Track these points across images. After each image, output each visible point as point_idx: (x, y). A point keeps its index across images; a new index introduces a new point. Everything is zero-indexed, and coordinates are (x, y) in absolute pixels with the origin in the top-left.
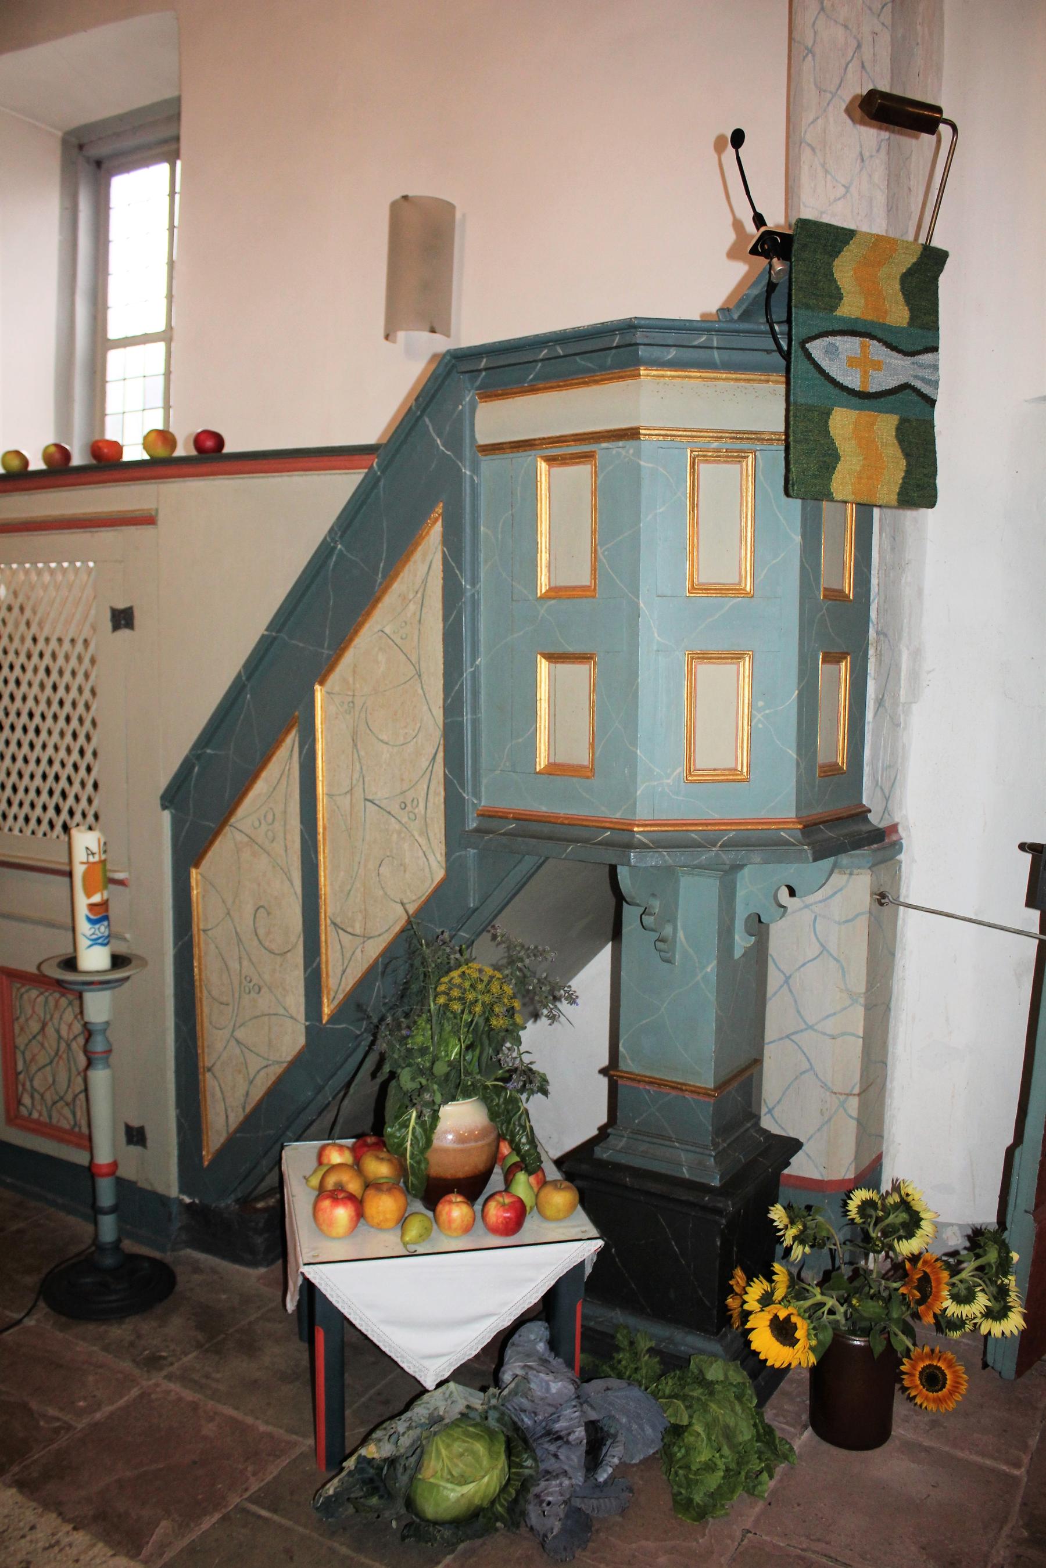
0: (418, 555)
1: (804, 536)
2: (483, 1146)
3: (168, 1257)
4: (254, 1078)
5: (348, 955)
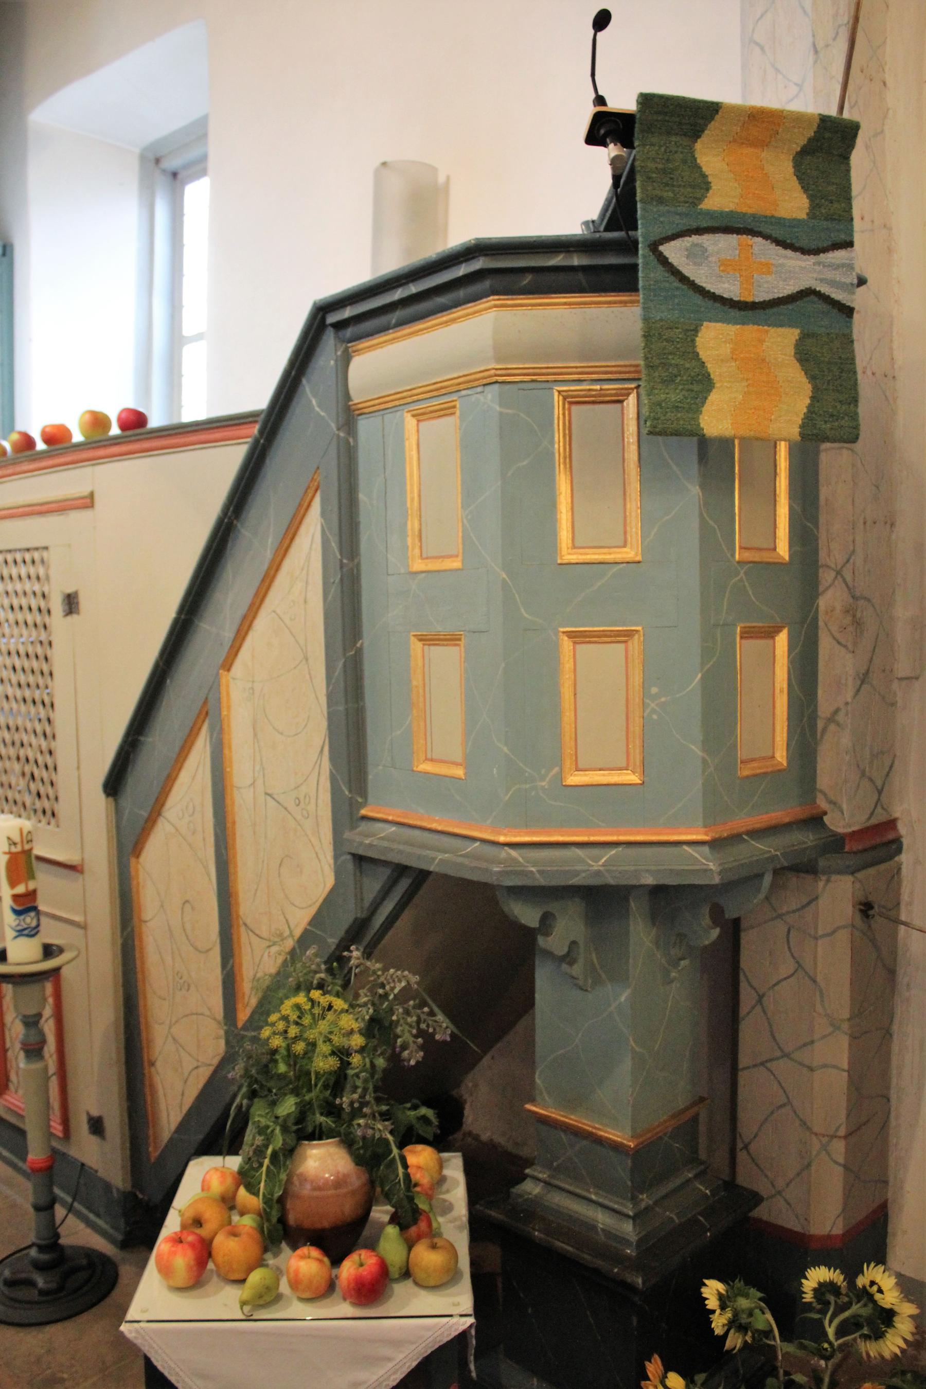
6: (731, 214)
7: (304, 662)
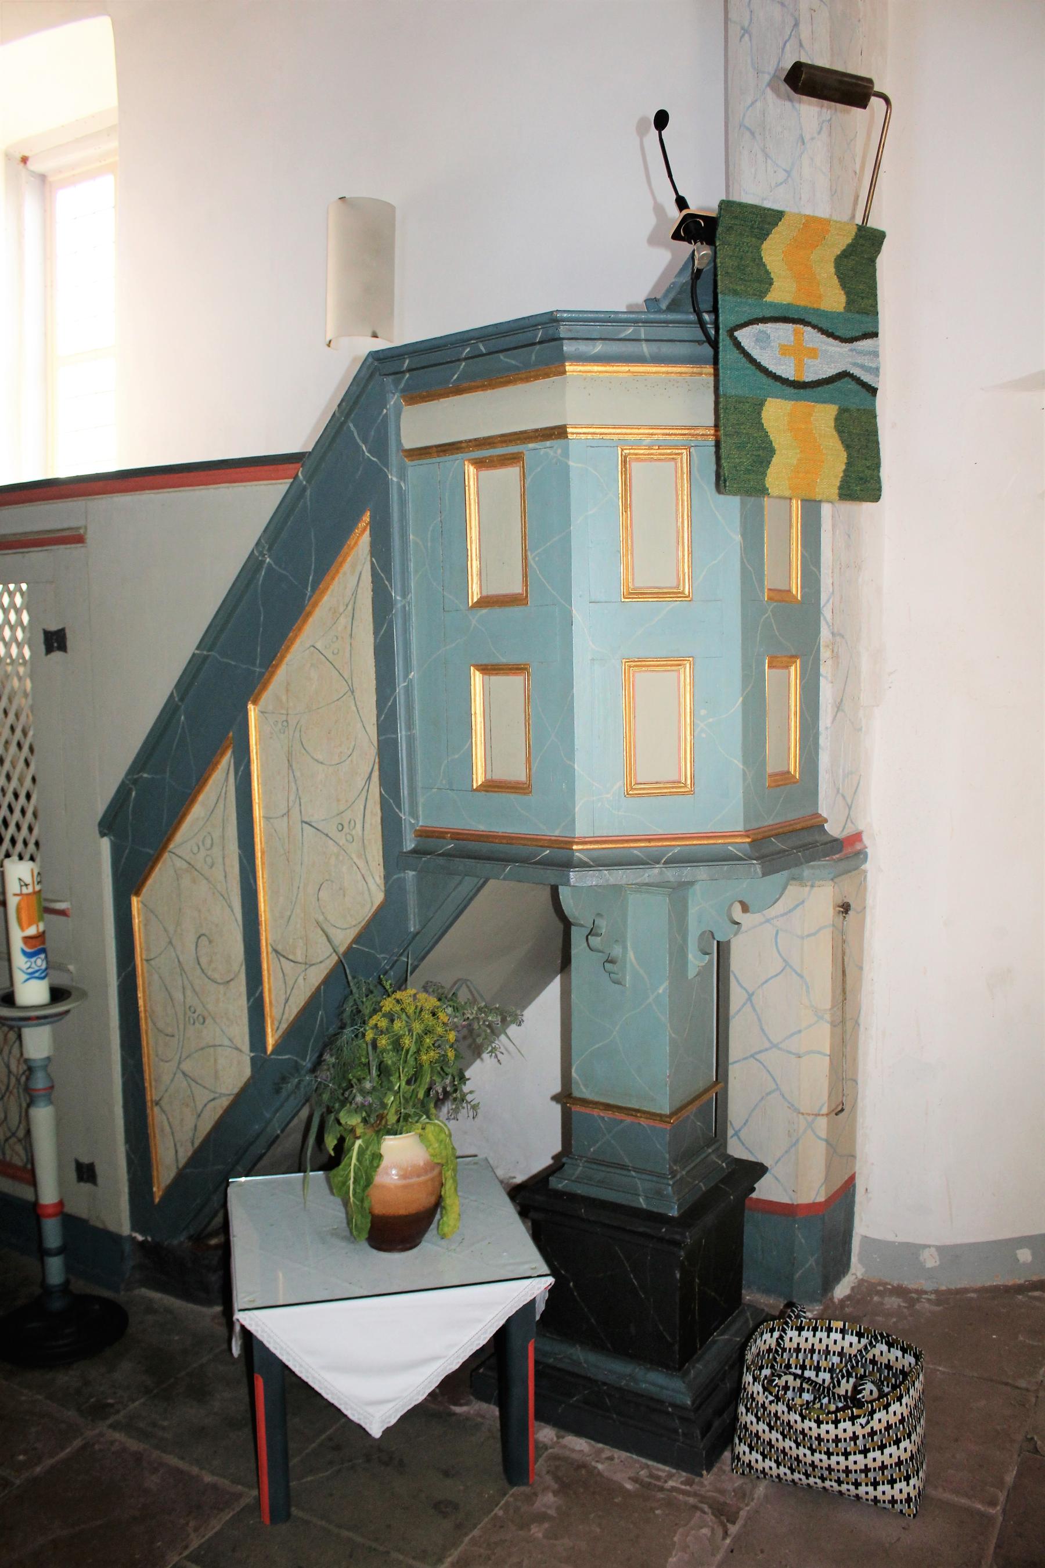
0: (346, 567)
1: (744, 535)
2: (425, 1183)
3: (121, 1297)
4: (202, 1112)
5: (290, 983)
6: (789, 306)
7: (350, 693)
